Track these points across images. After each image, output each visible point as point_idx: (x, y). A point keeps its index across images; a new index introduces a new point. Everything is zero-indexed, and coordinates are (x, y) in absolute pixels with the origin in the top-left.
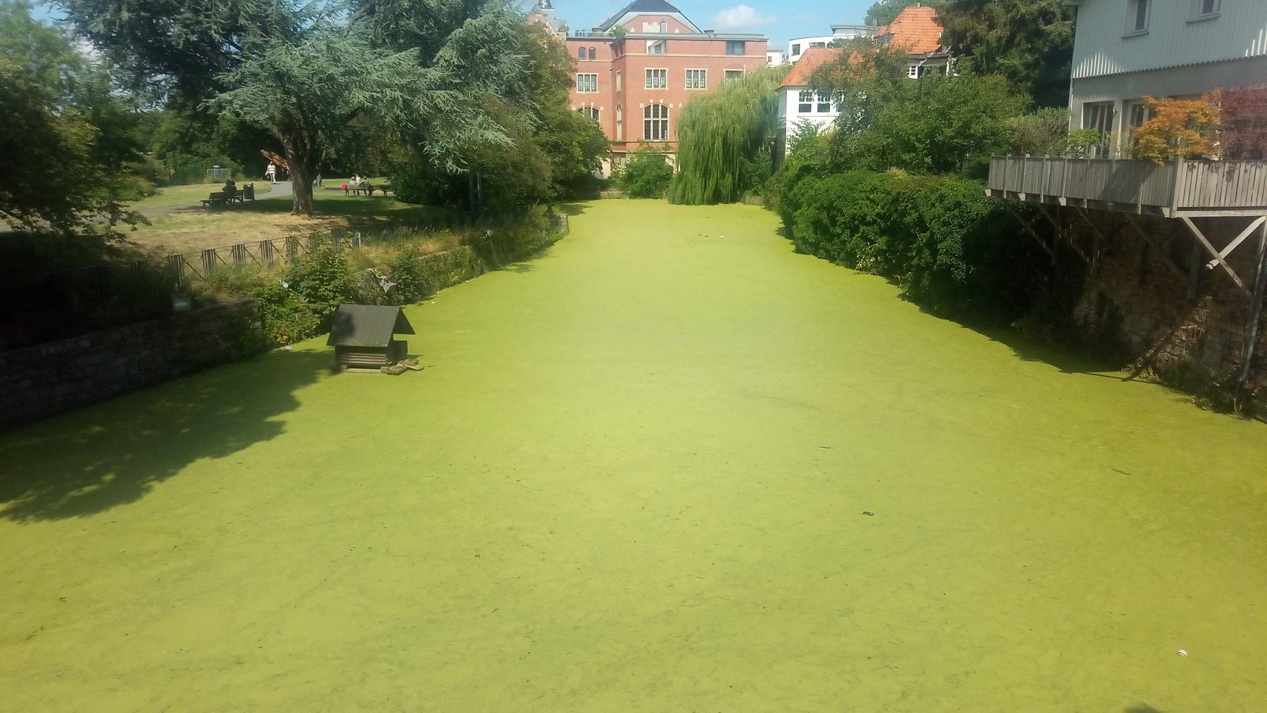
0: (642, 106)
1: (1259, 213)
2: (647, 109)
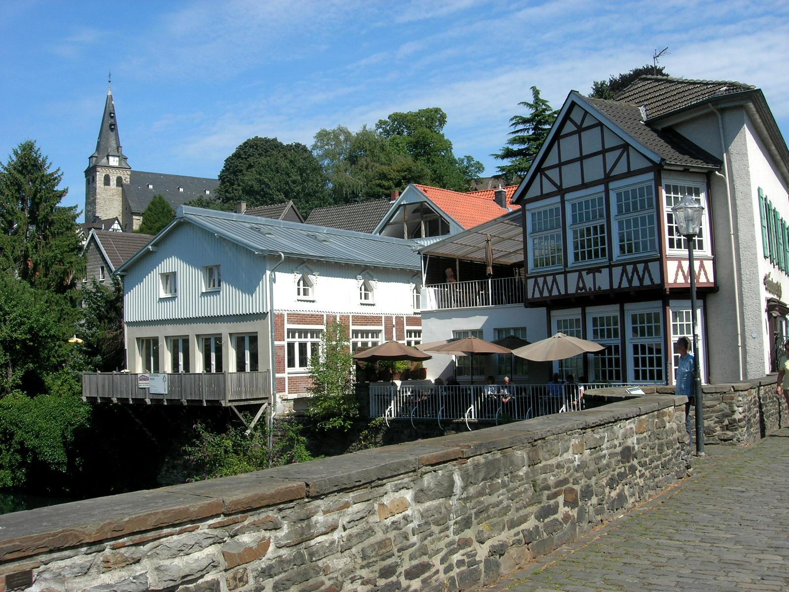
1: (263, 401)
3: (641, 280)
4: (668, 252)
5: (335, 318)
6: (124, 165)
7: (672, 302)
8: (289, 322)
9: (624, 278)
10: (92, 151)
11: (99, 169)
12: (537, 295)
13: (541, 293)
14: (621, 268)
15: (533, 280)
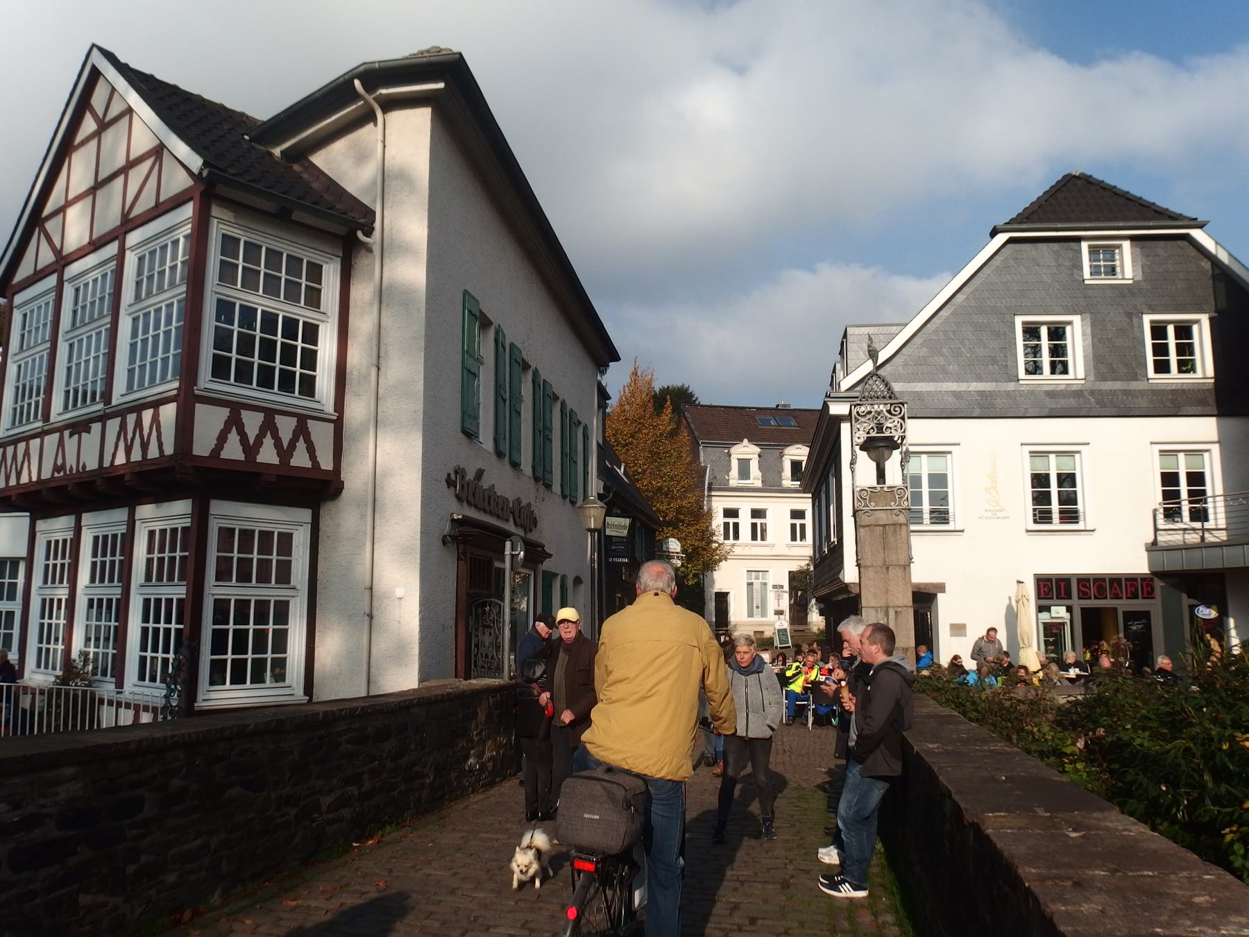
3: (285, 453)
9: (234, 437)
12: (233, 451)
14: (224, 413)
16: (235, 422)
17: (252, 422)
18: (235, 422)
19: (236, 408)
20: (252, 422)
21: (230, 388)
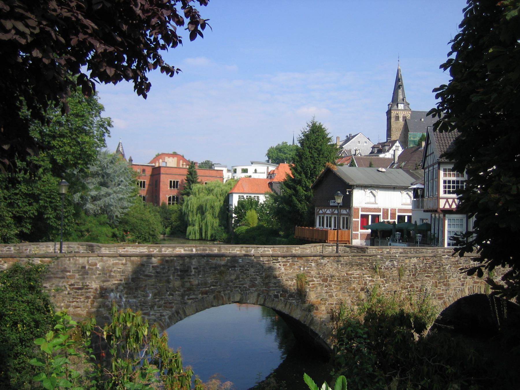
0: (168, 197)
2: (170, 198)
3: (450, 206)
4: (442, 194)
5: (388, 210)
6: (407, 108)
7: (447, 215)
8: (362, 211)
10: (390, 100)
11: (392, 111)
12: (447, 206)
13: (450, 206)
15: (445, 200)
16: (447, 201)
17: (450, 201)
18: (447, 201)
19: (447, 199)
20: (450, 201)
21: (447, 195)
